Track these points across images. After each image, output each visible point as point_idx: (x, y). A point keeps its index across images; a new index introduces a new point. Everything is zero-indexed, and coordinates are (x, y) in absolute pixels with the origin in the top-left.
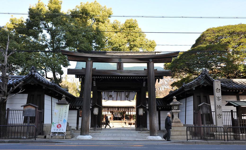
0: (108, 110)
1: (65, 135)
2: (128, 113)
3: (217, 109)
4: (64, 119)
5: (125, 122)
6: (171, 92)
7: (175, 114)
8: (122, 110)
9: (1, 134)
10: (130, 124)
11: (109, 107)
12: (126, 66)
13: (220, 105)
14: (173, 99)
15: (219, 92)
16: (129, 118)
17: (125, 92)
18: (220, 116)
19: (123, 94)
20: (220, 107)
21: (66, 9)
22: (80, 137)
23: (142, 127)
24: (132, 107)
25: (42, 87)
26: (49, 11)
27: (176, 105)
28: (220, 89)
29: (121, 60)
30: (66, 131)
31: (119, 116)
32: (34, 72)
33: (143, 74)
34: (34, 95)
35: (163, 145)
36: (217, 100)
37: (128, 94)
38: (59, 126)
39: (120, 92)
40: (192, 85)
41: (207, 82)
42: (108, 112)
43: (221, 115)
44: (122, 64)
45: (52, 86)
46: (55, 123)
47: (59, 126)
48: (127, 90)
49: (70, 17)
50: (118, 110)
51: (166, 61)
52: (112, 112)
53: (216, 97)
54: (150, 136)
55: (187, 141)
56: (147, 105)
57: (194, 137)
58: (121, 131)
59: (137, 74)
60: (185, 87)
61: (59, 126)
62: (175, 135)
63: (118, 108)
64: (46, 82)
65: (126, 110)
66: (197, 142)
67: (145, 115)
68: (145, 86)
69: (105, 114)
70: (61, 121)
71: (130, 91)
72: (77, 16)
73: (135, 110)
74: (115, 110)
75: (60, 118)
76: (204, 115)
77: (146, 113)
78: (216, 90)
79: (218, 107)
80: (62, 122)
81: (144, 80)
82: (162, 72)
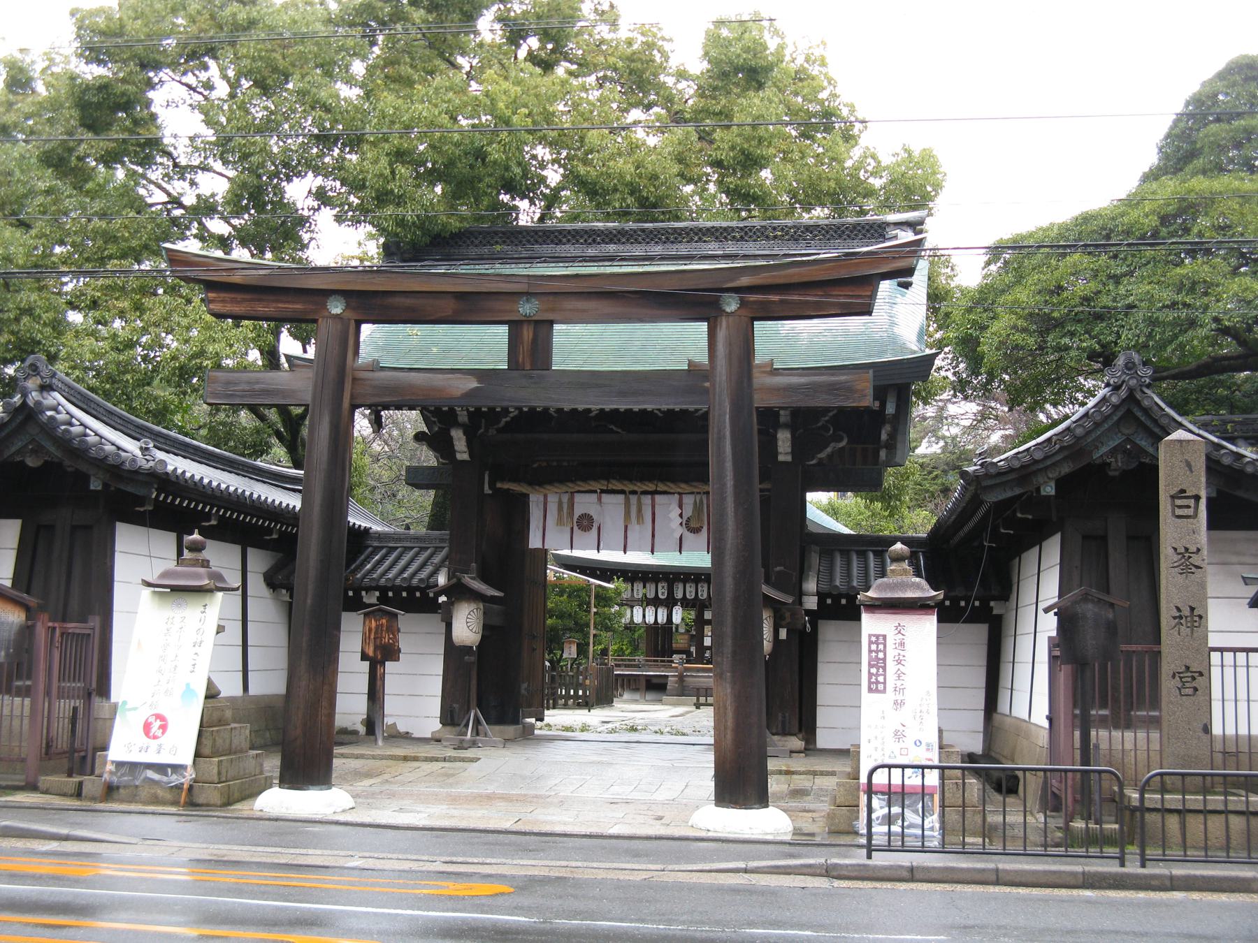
4: (188, 685)
9: (523, 692)
13: (1192, 609)
15: (1195, 515)
18: (1194, 678)
22: (278, 801)
25: (85, 479)
30: (198, 755)
38: (158, 723)
39: (645, 493)
43: (1201, 674)
46: (135, 709)
47: (156, 726)
55: (869, 857)
61: (158, 723)
68: (789, 458)
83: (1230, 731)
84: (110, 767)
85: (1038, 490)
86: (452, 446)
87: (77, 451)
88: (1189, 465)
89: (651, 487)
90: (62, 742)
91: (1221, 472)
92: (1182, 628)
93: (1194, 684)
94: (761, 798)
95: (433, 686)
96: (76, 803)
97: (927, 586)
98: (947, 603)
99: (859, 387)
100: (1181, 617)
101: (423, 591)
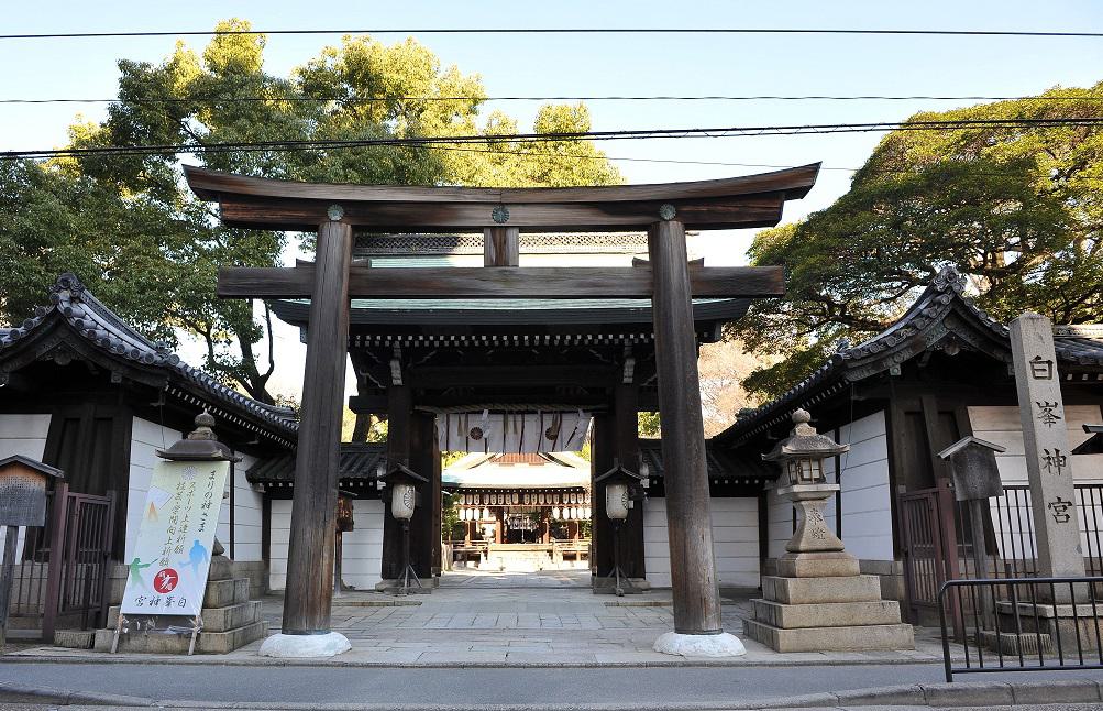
0: (482, 502)
1: (196, 629)
2: (561, 515)
3: (1044, 473)
4: (197, 542)
5: (551, 548)
6: (743, 414)
7: (808, 506)
8: (538, 503)
10: (569, 557)
11: (486, 489)
12: (537, 254)
13: (1057, 451)
15: (1050, 378)
16: (563, 531)
17: (542, 412)
18: (1065, 508)
19: (532, 426)
20: (1058, 460)
21: (282, 62)
22: (279, 644)
23: (620, 576)
24: (575, 488)
25: (108, 373)
26: (207, 71)
27: (818, 457)
28: (1050, 363)
29: (505, 212)
30: (205, 606)
31: (527, 525)
32: (72, 300)
33: (627, 285)
34: (78, 420)
37: (554, 423)
38: (169, 577)
39: (518, 413)
40: (889, 348)
41: (963, 336)
42: (481, 510)
43: (1070, 504)
45: (156, 371)
46: (148, 565)
47: (165, 581)
48: (549, 404)
49: (299, 91)
50: (521, 502)
51: (750, 215)
52: (498, 512)
53: (1035, 407)
54: (678, 631)
55: (949, 680)
56: (645, 471)
58: (523, 597)
59: (598, 289)
60: (853, 359)
61: (169, 577)
62: (821, 624)
63: (522, 492)
64: (123, 347)
65: (553, 503)
66: (1027, 690)
67: (636, 517)
69: (469, 519)
70: (179, 550)
71: (562, 408)
72: (328, 95)
73: (588, 501)
74: (509, 503)
75: (174, 538)
76: (974, 506)
77: (639, 504)
78: (1028, 366)
79: (1049, 458)
80: (185, 556)
81: (626, 354)
82: (729, 274)
84: (121, 619)
87: (101, 349)
89: (524, 408)
90: (78, 599)
93: (1067, 512)
96: (87, 654)
99: (775, 280)
101: (366, 482)
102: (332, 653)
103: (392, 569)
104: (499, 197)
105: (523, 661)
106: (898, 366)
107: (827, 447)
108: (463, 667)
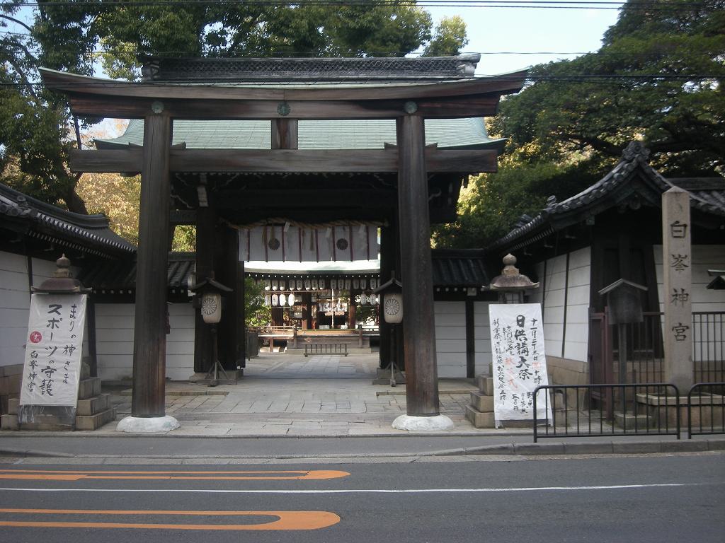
13: (683, 290)
14: (504, 266)
18: (684, 330)
22: (128, 423)
23: (394, 368)
28: (685, 226)
30: (79, 398)
35: (450, 465)
36: (674, 268)
44: (292, 124)
54: (410, 414)
55: (535, 441)
57: (584, 412)
83: (712, 359)
85: (584, 221)
86: (197, 197)
88: (681, 207)
91: (697, 213)
92: (678, 302)
93: (683, 334)
94: (436, 409)
95: (190, 348)
97: (527, 279)
98: (95, 292)
100: (676, 295)
101: (178, 289)
102: (168, 430)
103: (202, 365)
104: (282, 96)
105: (298, 434)
106: (593, 218)
107: (523, 285)
108: (258, 437)
